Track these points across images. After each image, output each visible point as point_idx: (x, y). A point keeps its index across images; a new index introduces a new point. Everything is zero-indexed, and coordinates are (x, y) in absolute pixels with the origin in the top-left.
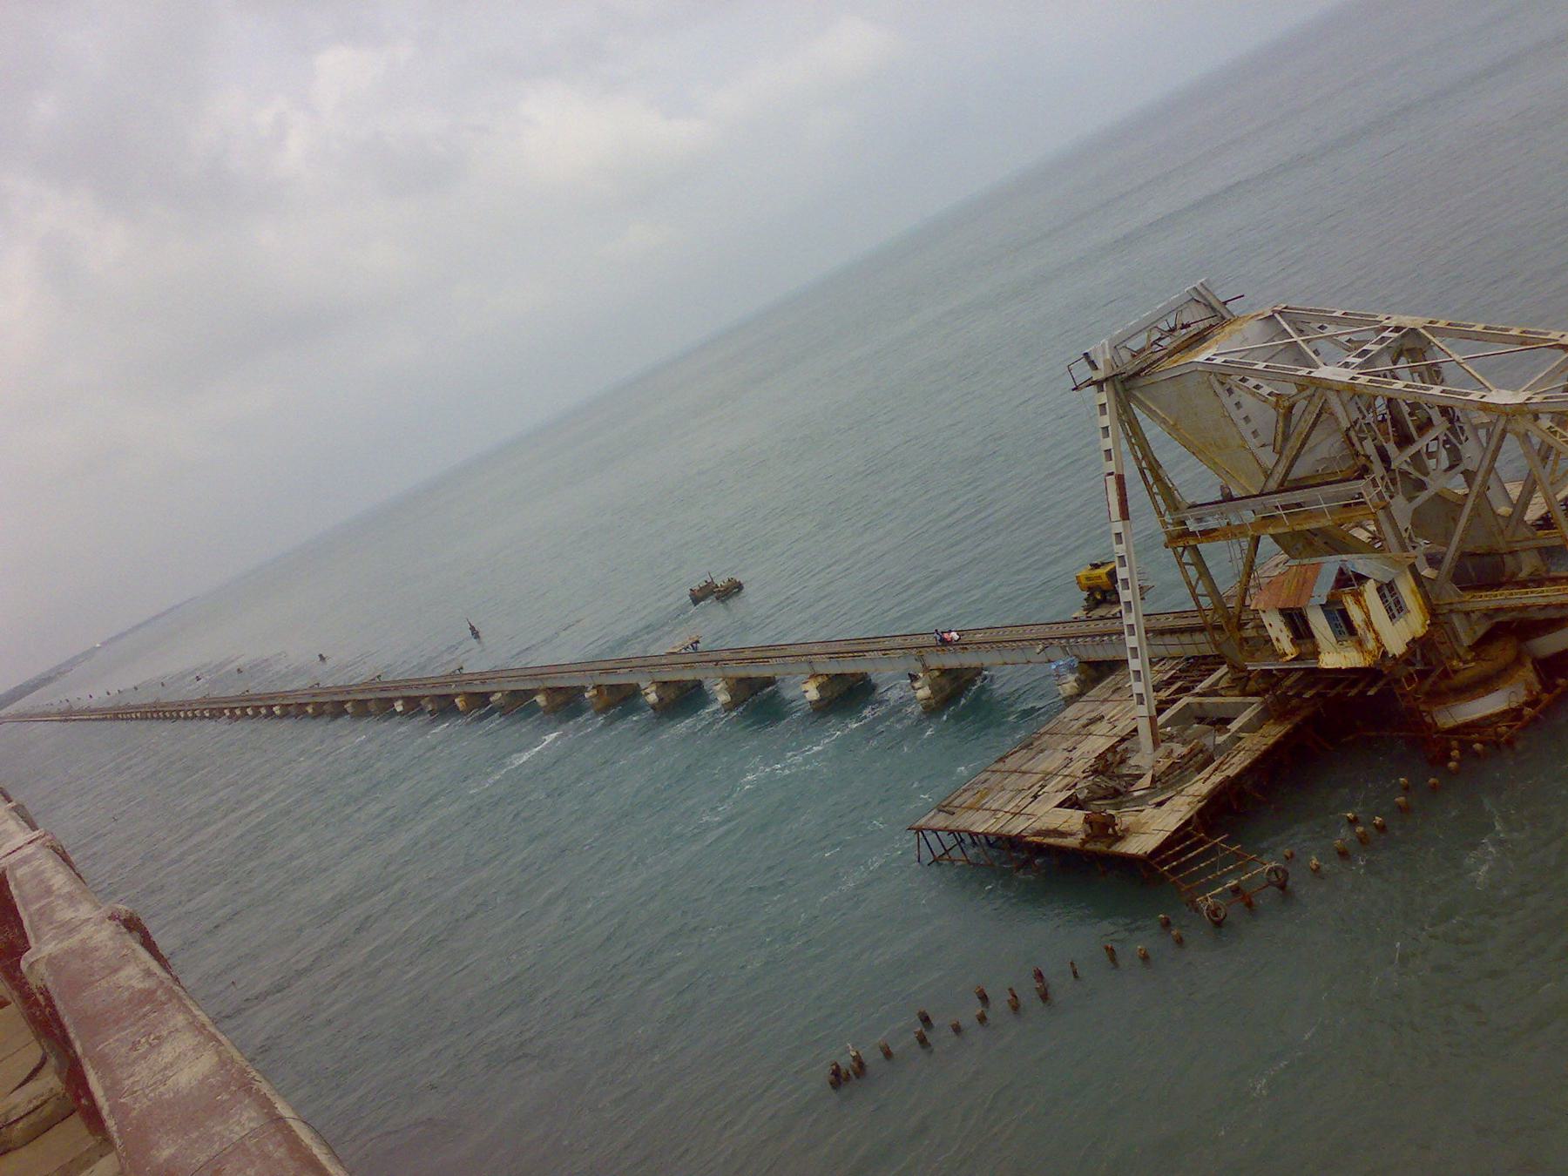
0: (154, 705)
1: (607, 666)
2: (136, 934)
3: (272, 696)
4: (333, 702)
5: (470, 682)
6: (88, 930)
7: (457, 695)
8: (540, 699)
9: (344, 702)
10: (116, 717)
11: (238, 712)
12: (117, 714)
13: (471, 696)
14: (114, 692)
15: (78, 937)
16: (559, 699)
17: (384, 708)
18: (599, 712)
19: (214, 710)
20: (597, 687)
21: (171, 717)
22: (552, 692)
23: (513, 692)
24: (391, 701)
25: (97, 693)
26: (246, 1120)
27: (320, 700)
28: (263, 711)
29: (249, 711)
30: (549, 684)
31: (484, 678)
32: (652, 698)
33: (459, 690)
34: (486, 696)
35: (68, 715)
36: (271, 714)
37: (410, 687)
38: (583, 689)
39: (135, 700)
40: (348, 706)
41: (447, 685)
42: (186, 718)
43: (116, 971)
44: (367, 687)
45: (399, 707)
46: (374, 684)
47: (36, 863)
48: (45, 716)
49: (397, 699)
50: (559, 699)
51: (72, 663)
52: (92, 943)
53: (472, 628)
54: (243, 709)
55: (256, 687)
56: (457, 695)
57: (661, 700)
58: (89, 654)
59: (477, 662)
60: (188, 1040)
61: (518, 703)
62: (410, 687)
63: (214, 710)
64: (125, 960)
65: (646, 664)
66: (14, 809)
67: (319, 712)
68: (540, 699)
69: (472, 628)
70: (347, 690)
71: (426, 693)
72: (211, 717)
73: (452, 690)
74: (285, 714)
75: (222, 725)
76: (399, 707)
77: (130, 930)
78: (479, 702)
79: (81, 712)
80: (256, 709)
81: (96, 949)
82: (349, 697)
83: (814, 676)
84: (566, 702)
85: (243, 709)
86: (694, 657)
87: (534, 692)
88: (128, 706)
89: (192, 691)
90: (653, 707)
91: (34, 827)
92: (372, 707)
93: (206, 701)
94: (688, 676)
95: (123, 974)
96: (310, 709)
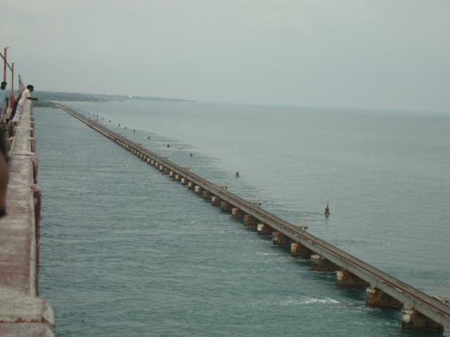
0: (138, 146)
1: (391, 280)
2: (36, 200)
3: (199, 180)
4: (228, 203)
5: (306, 239)
6: (20, 186)
7: (294, 242)
8: (339, 275)
9: (234, 207)
10: (115, 141)
11: (177, 177)
12: (117, 139)
13: (301, 247)
14: (122, 126)
15: (16, 186)
16: (350, 282)
17: (252, 223)
18: (368, 305)
19: (166, 168)
20: (377, 290)
21: (142, 159)
22: (348, 275)
23: (327, 261)
24: (258, 221)
25: (113, 121)
26: (24, 238)
27: (222, 197)
28: (190, 184)
29: (183, 180)
30: (350, 269)
31: (315, 242)
32: (407, 318)
33: (298, 239)
34: (311, 252)
35: (93, 124)
36: (192, 189)
37: (270, 219)
38: (368, 285)
39: (130, 138)
40: (234, 210)
41: (294, 232)
42: (149, 163)
43: (19, 200)
44: (249, 205)
45: (260, 228)
46: (255, 207)
47: (18, 187)
48: (81, 118)
49: (261, 222)
50: (350, 282)
51: (111, 98)
52: (19, 190)
53: (327, 210)
54: (181, 177)
55: (195, 169)
56: (294, 242)
57: (411, 322)
58: (122, 99)
59: (317, 229)
60: (24, 221)
61: (326, 268)
62: (273, 221)
63: (166, 168)
64: (24, 198)
65: (417, 296)
66: (31, 141)
67: (217, 204)
68: (339, 275)
69: (327, 210)
70: (239, 201)
71: (279, 229)
72: (162, 171)
73: (294, 237)
74: (200, 194)
75: (163, 179)
76: (260, 228)
77: (35, 197)
78: (304, 254)
79: (100, 127)
80: (187, 181)
81: (19, 192)
82: (237, 205)
83: (413, 309)
84: (352, 286)
85: (181, 177)
86: (224, 192)
87: (339, 268)
88: (124, 138)
89: (159, 150)
90: (404, 323)
91: (33, 150)
92: (246, 218)
93: (165, 161)
94: (437, 319)
95: (20, 202)
96: (213, 199)
